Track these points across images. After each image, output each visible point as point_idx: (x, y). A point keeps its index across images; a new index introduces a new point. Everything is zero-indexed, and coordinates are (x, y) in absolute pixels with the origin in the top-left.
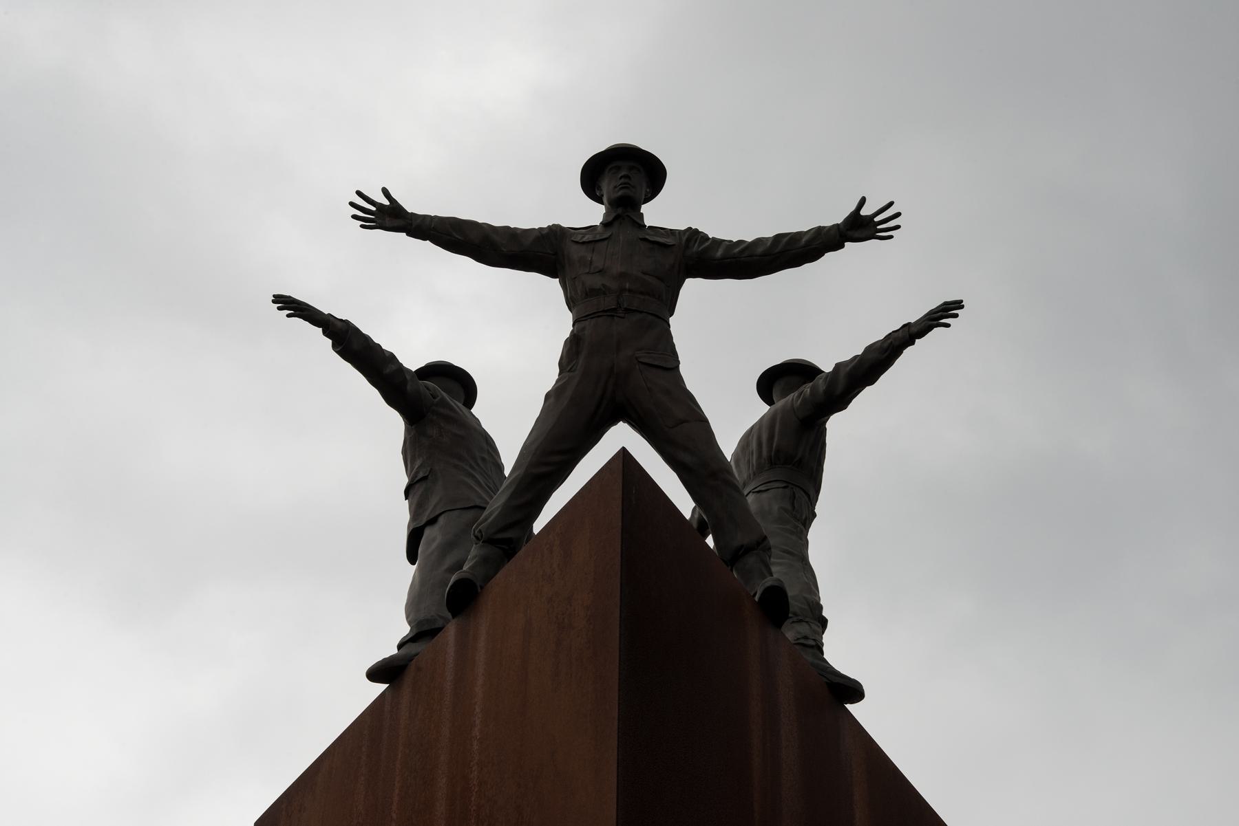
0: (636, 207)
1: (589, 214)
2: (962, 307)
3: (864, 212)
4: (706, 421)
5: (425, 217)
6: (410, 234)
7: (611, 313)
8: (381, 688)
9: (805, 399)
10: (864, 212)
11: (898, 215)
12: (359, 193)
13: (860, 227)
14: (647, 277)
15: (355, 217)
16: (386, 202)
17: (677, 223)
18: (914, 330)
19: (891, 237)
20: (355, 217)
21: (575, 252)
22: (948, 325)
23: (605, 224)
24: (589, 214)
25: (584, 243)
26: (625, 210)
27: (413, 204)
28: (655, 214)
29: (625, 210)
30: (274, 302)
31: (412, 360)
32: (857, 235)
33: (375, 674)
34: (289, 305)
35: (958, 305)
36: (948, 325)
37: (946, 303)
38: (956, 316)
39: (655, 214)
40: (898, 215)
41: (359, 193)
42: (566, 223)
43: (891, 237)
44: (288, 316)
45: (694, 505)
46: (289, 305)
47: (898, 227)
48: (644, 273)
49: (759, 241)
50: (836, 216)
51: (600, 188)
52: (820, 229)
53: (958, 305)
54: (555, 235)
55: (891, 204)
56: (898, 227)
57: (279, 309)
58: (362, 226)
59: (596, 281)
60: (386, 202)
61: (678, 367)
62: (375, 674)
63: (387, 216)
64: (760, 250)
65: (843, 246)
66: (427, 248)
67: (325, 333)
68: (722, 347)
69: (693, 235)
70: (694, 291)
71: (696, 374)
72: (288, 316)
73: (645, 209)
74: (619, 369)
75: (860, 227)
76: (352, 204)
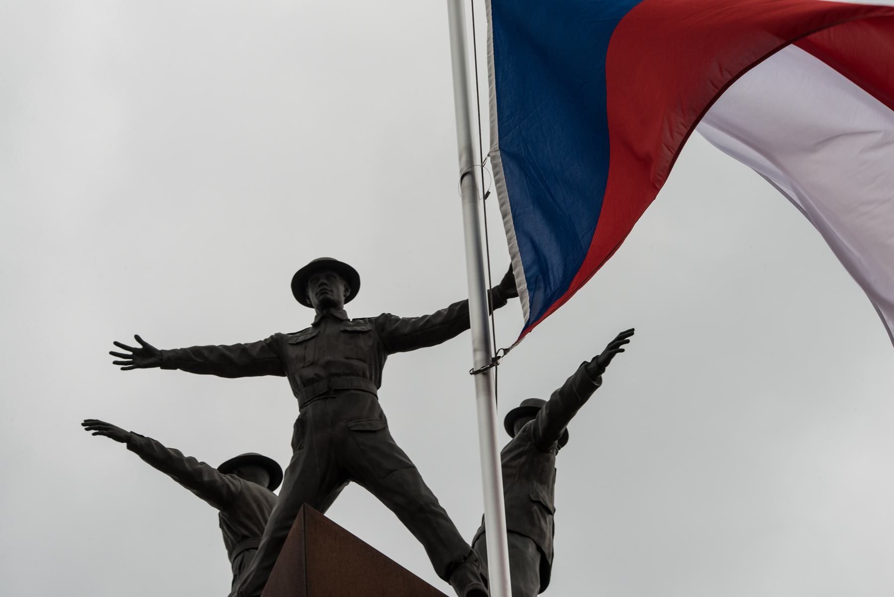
0: (337, 305)
1: (301, 318)
4: (413, 467)
5: (174, 351)
6: (164, 367)
7: (326, 396)
9: (536, 438)
12: (116, 344)
15: (115, 363)
16: (140, 346)
17: (374, 313)
18: (601, 360)
20: (115, 363)
21: (293, 352)
22: (623, 350)
23: (315, 325)
24: (301, 318)
25: (298, 344)
26: (329, 312)
27: (161, 343)
28: (354, 310)
29: (329, 312)
31: (214, 457)
34: (97, 427)
35: (631, 332)
39: (354, 310)
41: (116, 344)
42: (285, 331)
45: (219, 511)
46: (97, 427)
48: (347, 358)
49: (439, 313)
51: (309, 299)
53: (631, 332)
54: (277, 343)
58: (123, 369)
59: (309, 373)
60: (140, 346)
63: (143, 357)
64: (440, 319)
66: (179, 374)
67: (129, 448)
69: (386, 319)
71: (403, 432)
72: (94, 434)
73: (346, 307)
76: (112, 353)
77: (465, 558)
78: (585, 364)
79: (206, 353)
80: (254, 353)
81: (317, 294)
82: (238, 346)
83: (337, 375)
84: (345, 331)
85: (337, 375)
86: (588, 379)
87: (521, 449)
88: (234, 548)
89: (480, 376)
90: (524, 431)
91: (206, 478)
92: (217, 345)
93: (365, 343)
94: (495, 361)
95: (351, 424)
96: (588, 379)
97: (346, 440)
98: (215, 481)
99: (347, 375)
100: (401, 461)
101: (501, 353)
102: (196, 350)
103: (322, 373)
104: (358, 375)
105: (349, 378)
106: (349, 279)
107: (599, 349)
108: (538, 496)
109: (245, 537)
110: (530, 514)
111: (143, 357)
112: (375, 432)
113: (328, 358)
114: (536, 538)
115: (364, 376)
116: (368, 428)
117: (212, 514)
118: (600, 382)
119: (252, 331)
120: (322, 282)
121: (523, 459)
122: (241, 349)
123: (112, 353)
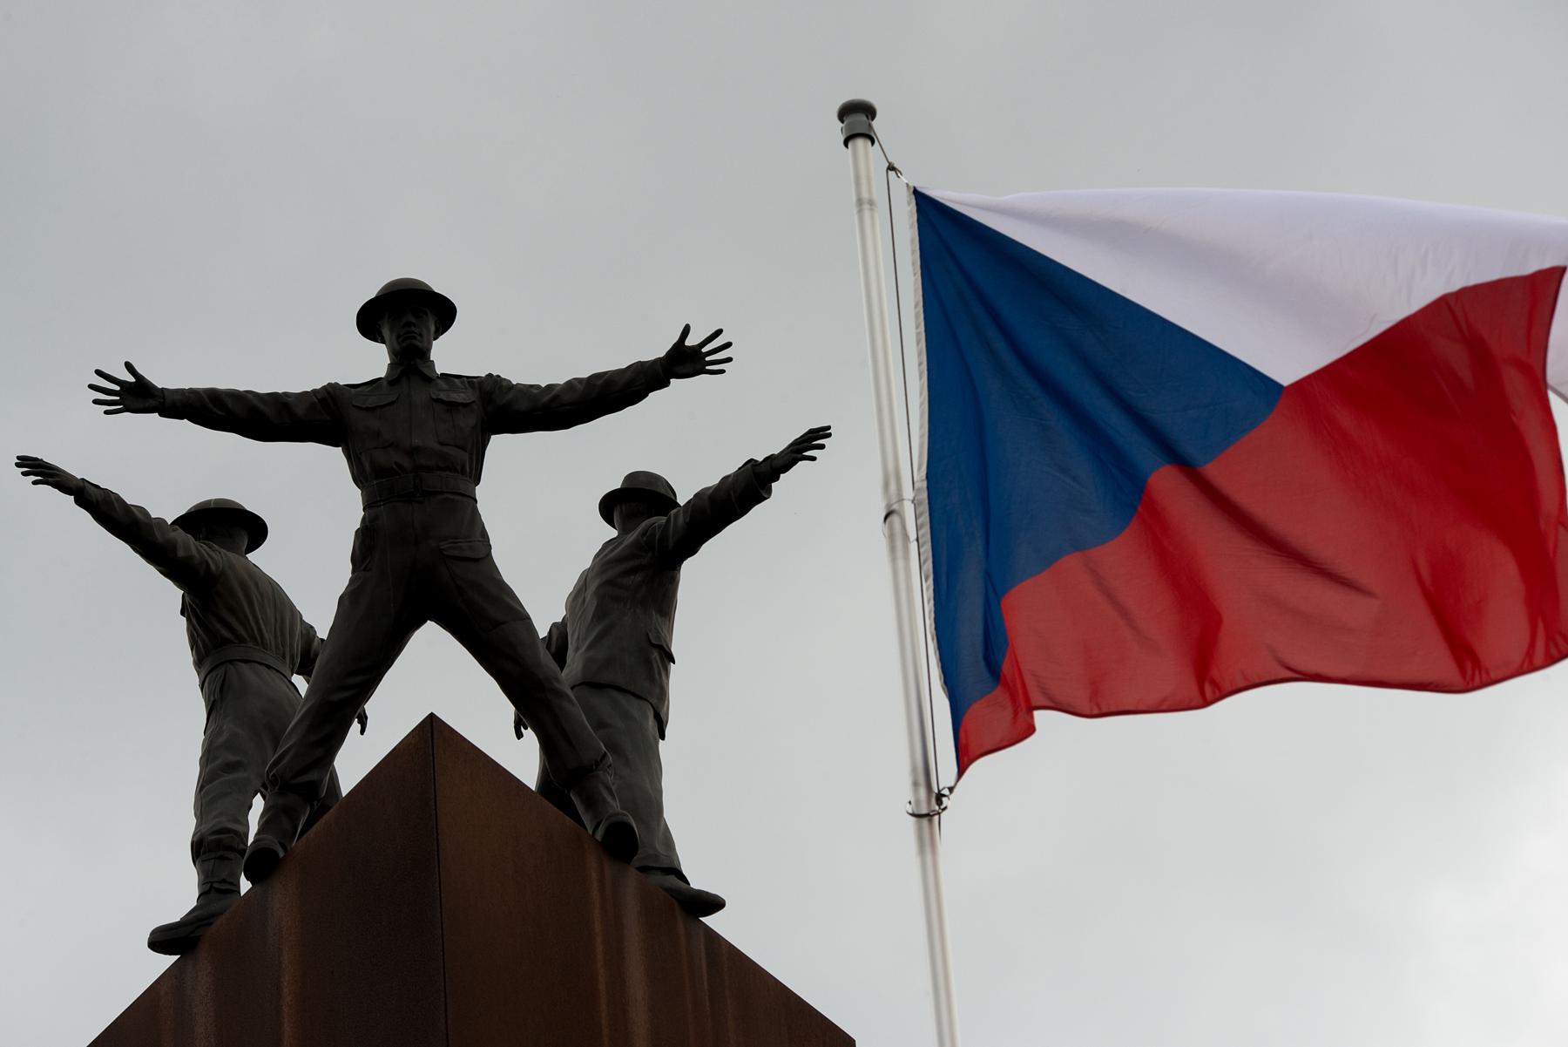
1: (369, 362)
2: (829, 435)
3: (689, 342)
8: (167, 961)
10: (689, 342)
11: (728, 345)
12: (99, 373)
13: (686, 360)
14: (446, 449)
15: (96, 402)
16: (132, 379)
19: (722, 372)
20: (96, 402)
22: (813, 459)
24: (369, 362)
25: (367, 409)
26: (410, 360)
27: (165, 377)
28: (451, 354)
29: (410, 360)
30: (18, 465)
32: (685, 370)
33: (161, 941)
36: (813, 459)
37: (811, 431)
38: (822, 447)
39: (451, 354)
40: (728, 345)
41: (99, 373)
43: (722, 372)
44: (35, 483)
47: (729, 360)
48: (442, 444)
50: (657, 349)
52: (640, 364)
55: (719, 332)
56: (729, 360)
57: (24, 474)
58: (106, 412)
60: (132, 379)
61: (489, 554)
62: (161, 941)
63: (135, 395)
64: (508, 600)
65: (667, 384)
67: (77, 502)
68: (539, 520)
70: (501, 448)
72: (35, 483)
74: (424, 566)
75: (686, 360)
76: (92, 387)
77: (597, 764)
78: (751, 462)
79: (230, 403)
80: (300, 410)
81: (398, 337)
82: (274, 396)
83: (429, 469)
84: (439, 401)
85: (429, 469)
86: (748, 488)
87: (631, 564)
88: (207, 654)
89: (925, 821)
90: (644, 534)
91: (181, 554)
92: (666, 815)
93: (468, 421)
94: (939, 797)
95: (444, 545)
96: (748, 488)
97: (424, 566)
98: (191, 558)
99: (440, 469)
100: (512, 609)
101: (946, 792)
102: (214, 395)
103: (406, 463)
104: (456, 470)
105: (444, 474)
106: (442, 312)
107: (777, 446)
108: (658, 638)
109: (225, 642)
110: (648, 663)
111: (135, 395)
112: (477, 560)
113: (417, 441)
114: (654, 701)
115: (463, 472)
116: (468, 554)
117: (171, 594)
118: (769, 492)
119: (297, 375)
120: (407, 314)
121: (639, 578)
122: (279, 401)
123: (92, 387)
